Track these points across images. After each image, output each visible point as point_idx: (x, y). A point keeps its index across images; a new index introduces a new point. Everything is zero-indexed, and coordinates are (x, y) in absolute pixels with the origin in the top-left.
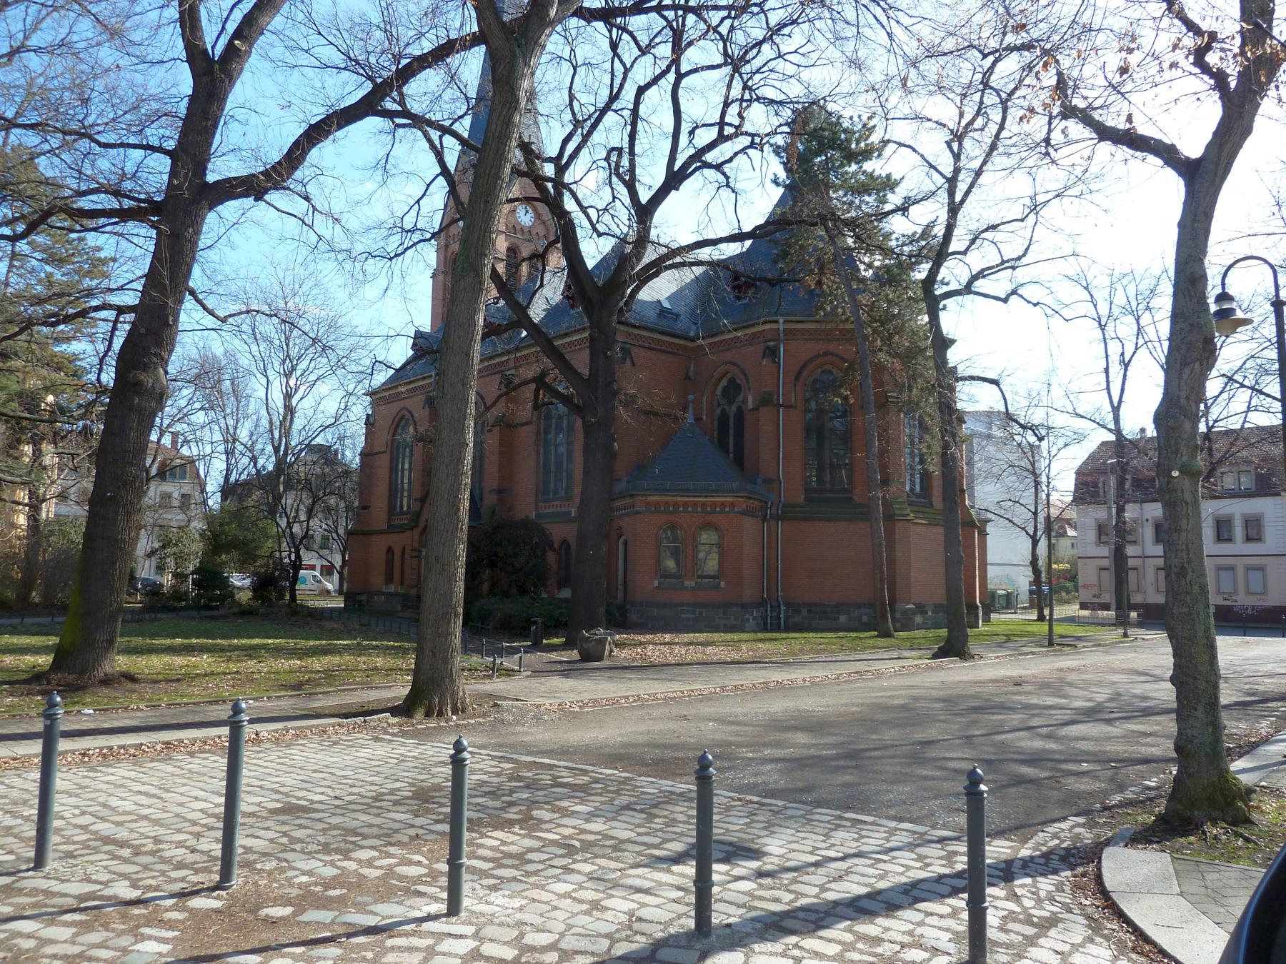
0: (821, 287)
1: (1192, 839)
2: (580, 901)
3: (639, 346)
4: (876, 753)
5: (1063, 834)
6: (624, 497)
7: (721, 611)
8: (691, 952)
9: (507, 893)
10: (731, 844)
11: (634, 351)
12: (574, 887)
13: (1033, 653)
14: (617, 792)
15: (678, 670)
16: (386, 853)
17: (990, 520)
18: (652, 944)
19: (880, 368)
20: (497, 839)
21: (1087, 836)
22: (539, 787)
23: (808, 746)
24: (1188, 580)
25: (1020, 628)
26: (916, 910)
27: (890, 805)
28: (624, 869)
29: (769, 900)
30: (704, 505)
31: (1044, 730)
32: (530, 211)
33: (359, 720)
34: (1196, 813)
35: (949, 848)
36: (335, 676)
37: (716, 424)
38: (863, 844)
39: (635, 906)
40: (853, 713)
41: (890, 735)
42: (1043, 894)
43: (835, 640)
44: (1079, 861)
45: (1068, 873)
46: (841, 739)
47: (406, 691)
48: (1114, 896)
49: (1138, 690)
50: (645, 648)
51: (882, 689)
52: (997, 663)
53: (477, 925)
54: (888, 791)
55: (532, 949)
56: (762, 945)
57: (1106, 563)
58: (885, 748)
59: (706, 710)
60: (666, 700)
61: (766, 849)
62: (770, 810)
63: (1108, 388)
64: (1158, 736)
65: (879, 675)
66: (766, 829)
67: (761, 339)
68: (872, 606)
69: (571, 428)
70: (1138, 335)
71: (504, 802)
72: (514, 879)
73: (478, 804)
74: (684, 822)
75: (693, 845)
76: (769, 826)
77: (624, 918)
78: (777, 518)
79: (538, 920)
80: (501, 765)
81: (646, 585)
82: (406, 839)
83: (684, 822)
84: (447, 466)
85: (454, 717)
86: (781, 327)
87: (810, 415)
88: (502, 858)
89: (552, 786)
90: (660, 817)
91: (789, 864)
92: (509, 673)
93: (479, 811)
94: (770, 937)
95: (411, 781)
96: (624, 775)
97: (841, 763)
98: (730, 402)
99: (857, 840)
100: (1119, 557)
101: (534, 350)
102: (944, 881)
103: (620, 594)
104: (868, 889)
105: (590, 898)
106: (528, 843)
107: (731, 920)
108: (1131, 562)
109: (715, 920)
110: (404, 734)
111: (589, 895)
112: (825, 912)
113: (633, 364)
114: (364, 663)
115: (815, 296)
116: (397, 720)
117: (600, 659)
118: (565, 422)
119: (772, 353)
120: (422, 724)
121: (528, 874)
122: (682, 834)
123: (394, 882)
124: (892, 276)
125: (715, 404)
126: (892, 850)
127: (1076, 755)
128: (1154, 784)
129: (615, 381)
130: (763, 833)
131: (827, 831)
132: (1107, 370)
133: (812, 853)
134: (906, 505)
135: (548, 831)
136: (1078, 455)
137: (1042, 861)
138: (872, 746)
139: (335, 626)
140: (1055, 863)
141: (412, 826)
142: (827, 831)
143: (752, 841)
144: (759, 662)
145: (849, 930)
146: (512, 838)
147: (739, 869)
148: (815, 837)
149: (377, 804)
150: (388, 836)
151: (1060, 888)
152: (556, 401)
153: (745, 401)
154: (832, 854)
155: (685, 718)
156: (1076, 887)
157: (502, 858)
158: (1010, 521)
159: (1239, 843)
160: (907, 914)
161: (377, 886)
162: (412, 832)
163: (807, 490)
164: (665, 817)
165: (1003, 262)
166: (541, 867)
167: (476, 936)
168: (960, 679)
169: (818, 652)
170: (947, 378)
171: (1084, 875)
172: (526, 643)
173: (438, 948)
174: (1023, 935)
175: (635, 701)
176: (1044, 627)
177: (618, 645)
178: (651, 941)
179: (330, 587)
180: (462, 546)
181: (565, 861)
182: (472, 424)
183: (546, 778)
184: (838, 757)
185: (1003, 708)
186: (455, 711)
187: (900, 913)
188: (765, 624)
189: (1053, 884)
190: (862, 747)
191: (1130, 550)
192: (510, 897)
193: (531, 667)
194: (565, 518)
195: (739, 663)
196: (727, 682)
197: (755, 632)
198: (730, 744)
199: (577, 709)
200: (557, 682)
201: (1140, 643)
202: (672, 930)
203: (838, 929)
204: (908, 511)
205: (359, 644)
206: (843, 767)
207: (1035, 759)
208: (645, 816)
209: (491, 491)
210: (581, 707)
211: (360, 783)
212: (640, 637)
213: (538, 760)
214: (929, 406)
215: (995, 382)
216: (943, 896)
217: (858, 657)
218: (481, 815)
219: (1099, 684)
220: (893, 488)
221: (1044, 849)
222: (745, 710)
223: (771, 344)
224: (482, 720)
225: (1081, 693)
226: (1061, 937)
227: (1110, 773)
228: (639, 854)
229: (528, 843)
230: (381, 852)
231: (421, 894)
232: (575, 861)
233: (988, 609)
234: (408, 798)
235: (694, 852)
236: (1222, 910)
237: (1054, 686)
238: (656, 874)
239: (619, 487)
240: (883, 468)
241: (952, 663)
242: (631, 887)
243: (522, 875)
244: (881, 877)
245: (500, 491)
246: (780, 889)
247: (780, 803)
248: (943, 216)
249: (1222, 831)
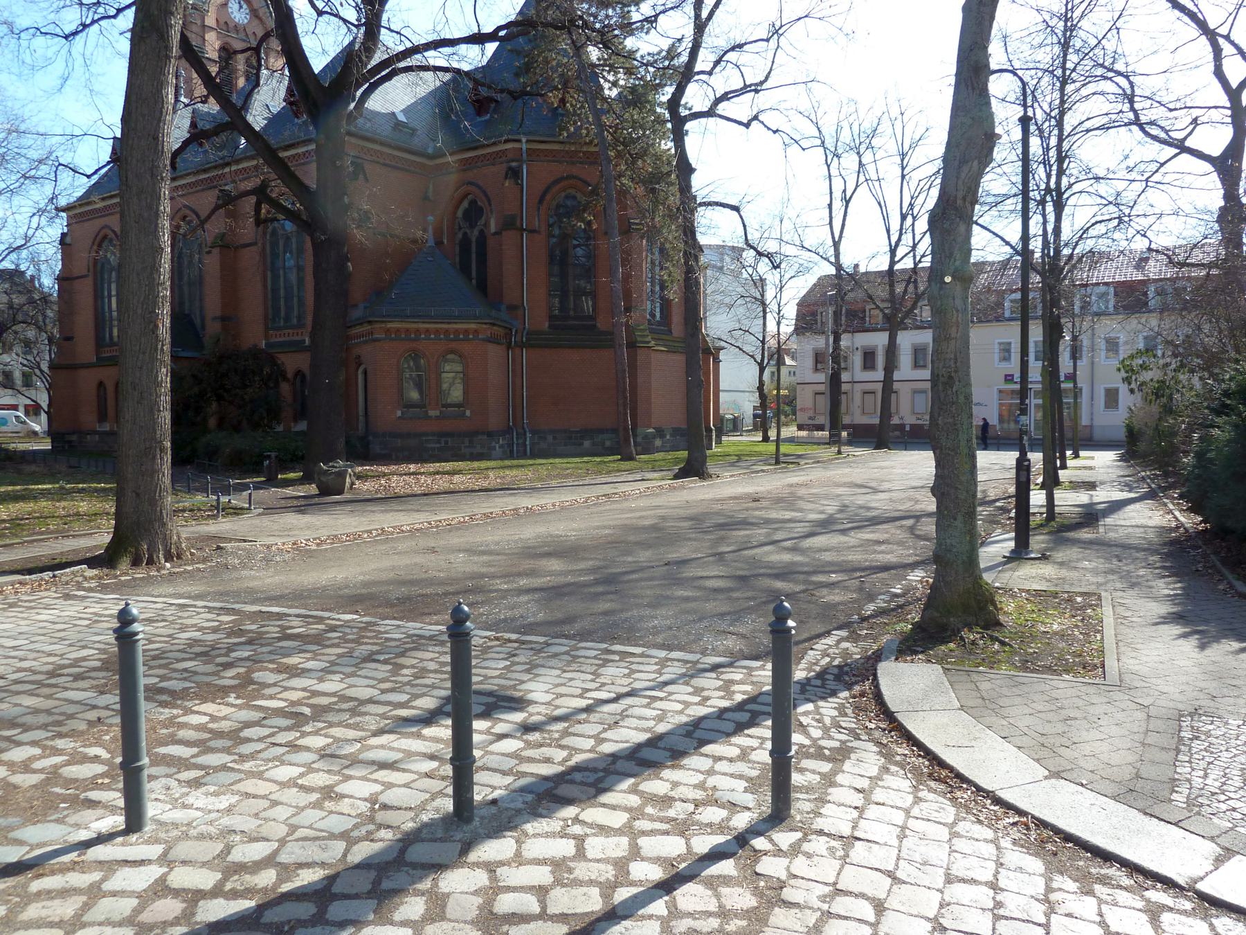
0: (565, 105)
1: (952, 645)
2: (307, 789)
3: (373, 161)
4: (634, 576)
5: (831, 651)
6: (361, 324)
7: (467, 440)
8: (448, 845)
9: (212, 789)
10: (490, 694)
11: (367, 167)
12: (302, 770)
13: (763, 471)
14: (357, 642)
15: (424, 500)
16: (52, 748)
17: (723, 348)
18: (399, 840)
19: (623, 193)
20: (205, 714)
21: (855, 651)
22: (263, 642)
23: (561, 573)
24: (954, 390)
25: (748, 449)
26: (702, 755)
27: (656, 631)
28: (365, 739)
29: (539, 761)
30: (447, 332)
31: (788, 544)
32: (245, 6)
33: (47, 575)
34: (952, 619)
35: (723, 677)
36: (23, 525)
37: (457, 249)
38: (635, 680)
39: (378, 788)
40: (606, 536)
41: (644, 556)
42: (828, 721)
43: (581, 465)
44: (854, 679)
45: (845, 694)
46: (597, 563)
47: (107, 539)
48: (899, 717)
49: (861, 500)
50: (389, 479)
51: (632, 510)
52: (733, 481)
53: (166, 842)
54: (652, 617)
55: (241, 868)
56: (535, 824)
57: (822, 388)
58: (642, 569)
59: (455, 540)
60: (413, 532)
61: (530, 696)
62: (532, 649)
63: (831, 223)
64: (890, 543)
65: (625, 497)
66: (528, 671)
67: (504, 158)
68: (614, 431)
69: (300, 251)
70: (859, 172)
71: (218, 665)
72: (224, 768)
73: (185, 670)
74: (436, 671)
75: (447, 700)
76: (531, 668)
77: (364, 807)
78: (521, 346)
79: (250, 824)
80: (220, 618)
81: (388, 415)
82: (83, 726)
83: (436, 671)
84: (138, 274)
85: (168, 565)
86: (524, 147)
87: (554, 240)
88: (210, 739)
89: (280, 639)
90: (408, 667)
91: (558, 712)
92: (237, 511)
93: (185, 679)
94: (544, 812)
95: (102, 646)
96: (365, 619)
97: (600, 589)
98: (472, 226)
99: (628, 676)
100: (835, 381)
101: (254, 163)
102: (726, 716)
103: (361, 426)
104: (648, 735)
105: (321, 784)
106: (246, 715)
107: (497, 794)
108: (844, 387)
109: (478, 796)
110: (104, 589)
111: (319, 779)
112: (604, 770)
113: (367, 180)
114: (64, 508)
115: (558, 114)
116: (95, 572)
117: (340, 492)
118: (294, 240)
119: (515, 174)
120: (127, 574)
121: (243, 758)
122: (433, 687)
123: (58, 790)
124: (637, 98)
125: (457, 227)
126: (666, 684)
127: (823, 566)
128: (899, 591)
129: (346, 194)
130: (526, 677)
131: (595, 668)
132: (830, 206)
133: (581, 696)
134: (647, 333)
135: (271, 697)
136: (798, 288)
137: (819, 682)
138: (629, 569)
139: (37, 469)
140: (832, 684)
141: (94, 707)
142: (595, 668)
143: (514, 687)
144: (508, 489)
145: (634, 790)
146: (225, 711)
147: (501, 724)
148: (584, 676)
149: (53, 681)
150: (59, 723)
151: (841, 710)
152: (281, 217)
153: (487, 224)
154: (604, 695)
155: (433, 551)
156: (858, 709)
157: (210, 739)
158: (740, 349)
159: (996, 647)
160: (694, 761)
161: (32, 798)
162: (92, 715)
163: (552, 318)
164: (413, 667)
165: (746, 86)
166: (260, 746)
167: (164, 859)
168: (701, 497)
169: (566, 476)
170: (688, 204)
171: (862, 694)
172: (259, 479)
173: (106, 886)
174: (819, 773)
175: (379, 535)
176: (771, 448)
177: (359, 477)
178: (399, 836)
179: (37, 428)
180: (164, 370)
181: (290, 736)
182: (167, 224)
183: (273, 630)
184: (597, 582)
185: (745, 523)
186: (168, 558)
187: (686, 761)
188: (511, 452)
189: (835, 708)
190: (619, 570)
191: (845, 377)
192: (216, 794)
193: (262, 503)
194: (297, 347)
195: (486, 490)
196: (476, 511)
197: (501, 459)
198: (482, 576)
199: (314, 547)
200: (292, 519)
201: (851, 459)
202: (425, 818)
203: (621, 791)
204: (649, 339)
205: (62, 488)
206: (603, 594)
207: (785, 573)
208: (389, 667)
209: (215, 318)
210: (318, 545)
211: (35, 655)
212: (384, 469)
213: (264, 609)
214: (671, 233)
215: (736, 209)
216: (729, 735)
217: (604, 480)
218: (188, 684)
219: (826, 497)
220: (635, 315)
221: (818, 669)
222: (496, 538)
223: (514, 164)
224: (201, 566)
225: (810, 506)
226: (857, 770)
227: (857, 582)
228: (384, 716)
229: (246, 715)
230: (44, 748)
231: (92, 804)
232: (304, 735)
233: (720, 433)
234: (95, 669)
235: (449, 708)
236: (1005, 723)
237: (787, 500)
238: (403, 741)
239: (356, 314)
240: (627, 295)
241: (692, 483)
242: (373, 763)
243: (234, 761)
244: (660, 719)
245: (224, 319)
246: (550, 745)
247: (541, 639)
248: (689, 31)
249: (978, 636)
